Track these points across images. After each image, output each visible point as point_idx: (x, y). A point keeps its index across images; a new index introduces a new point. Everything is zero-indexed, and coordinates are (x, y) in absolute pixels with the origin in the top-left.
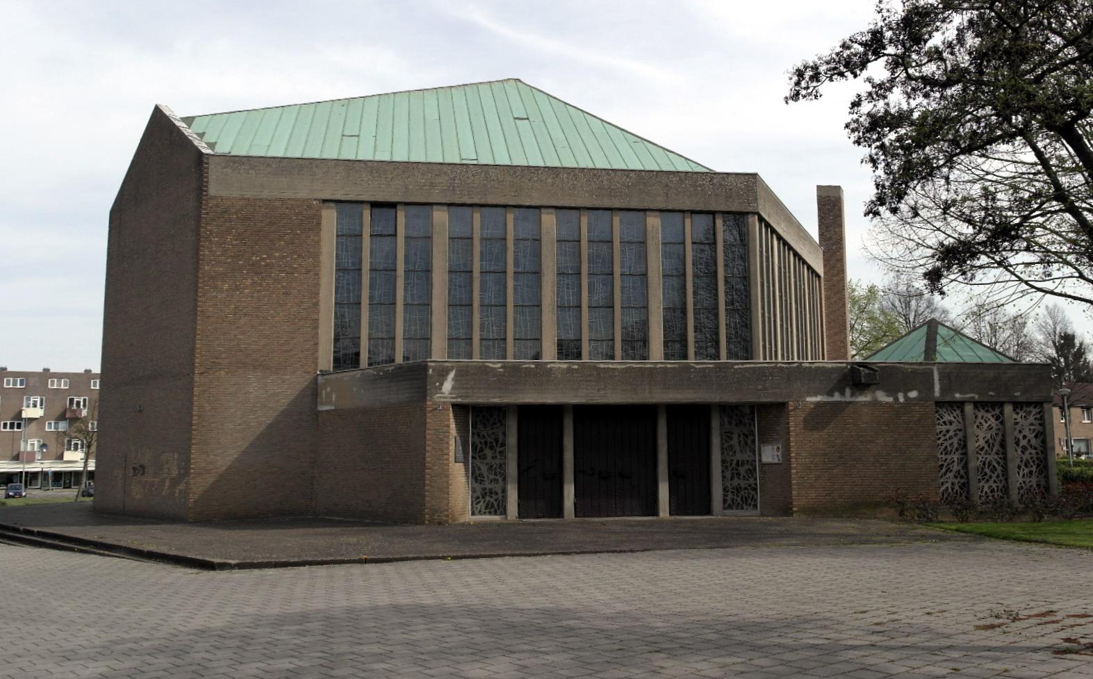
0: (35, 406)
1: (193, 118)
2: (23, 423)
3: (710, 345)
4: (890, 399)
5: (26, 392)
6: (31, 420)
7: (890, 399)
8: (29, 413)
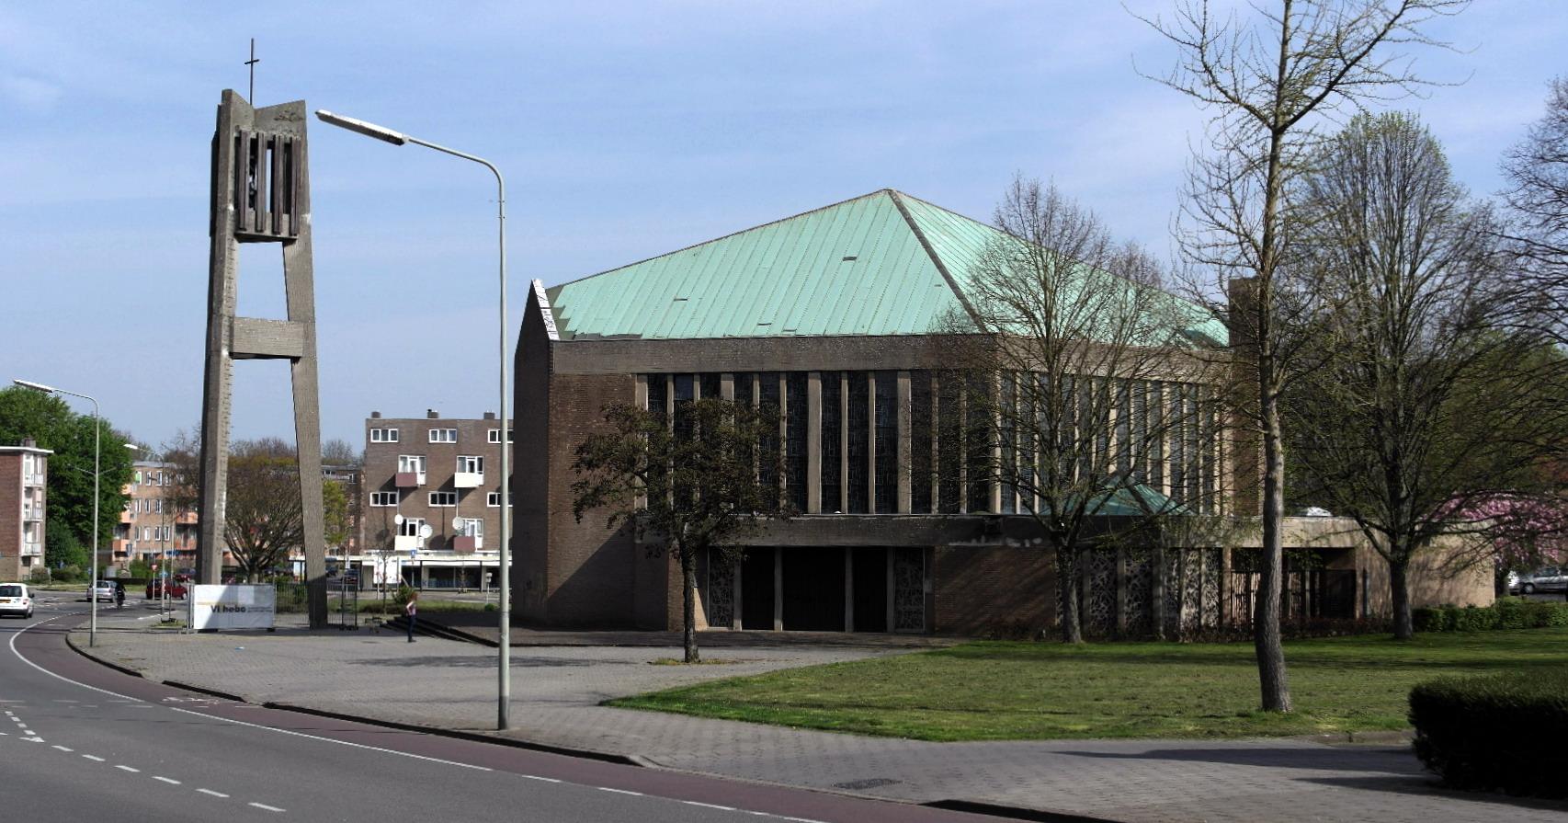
0: (472, 470)
1: (560, 288)
2: (457, 494)
3: (860, 502)
4: (1017, 545)
5: (459, 450)
6: (465, 491)
7: (1017, 545)
8: (464, 479)
